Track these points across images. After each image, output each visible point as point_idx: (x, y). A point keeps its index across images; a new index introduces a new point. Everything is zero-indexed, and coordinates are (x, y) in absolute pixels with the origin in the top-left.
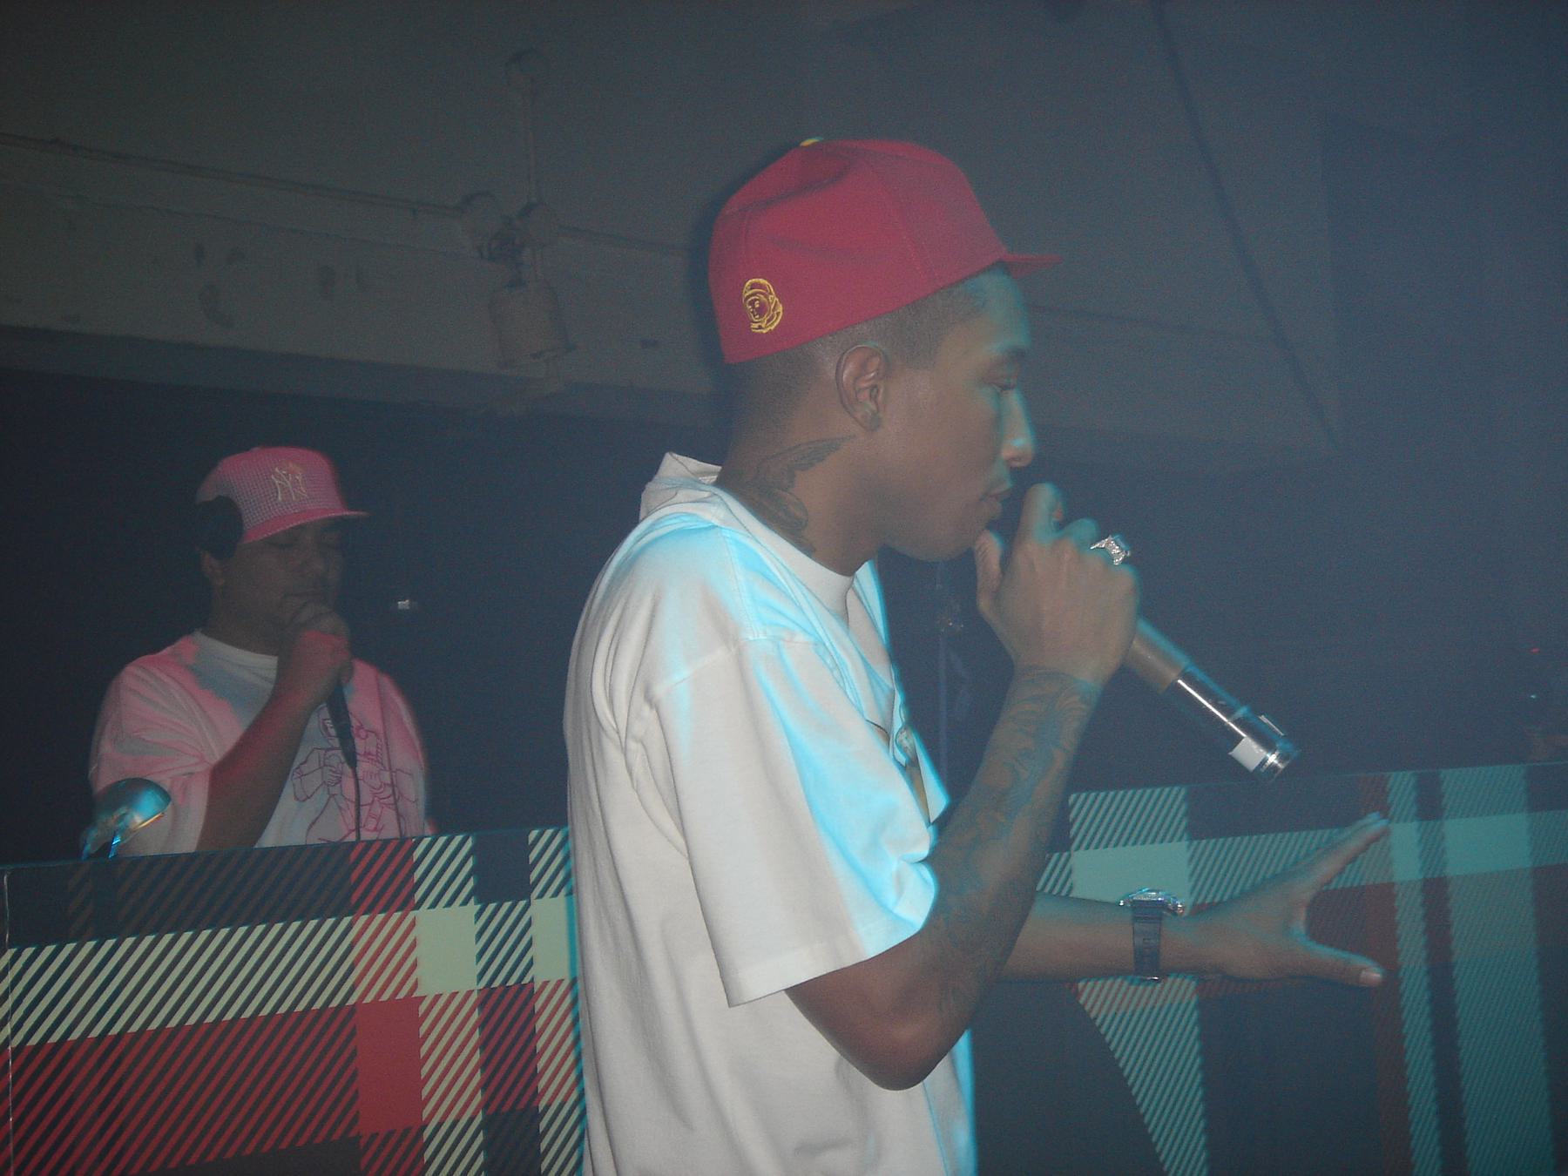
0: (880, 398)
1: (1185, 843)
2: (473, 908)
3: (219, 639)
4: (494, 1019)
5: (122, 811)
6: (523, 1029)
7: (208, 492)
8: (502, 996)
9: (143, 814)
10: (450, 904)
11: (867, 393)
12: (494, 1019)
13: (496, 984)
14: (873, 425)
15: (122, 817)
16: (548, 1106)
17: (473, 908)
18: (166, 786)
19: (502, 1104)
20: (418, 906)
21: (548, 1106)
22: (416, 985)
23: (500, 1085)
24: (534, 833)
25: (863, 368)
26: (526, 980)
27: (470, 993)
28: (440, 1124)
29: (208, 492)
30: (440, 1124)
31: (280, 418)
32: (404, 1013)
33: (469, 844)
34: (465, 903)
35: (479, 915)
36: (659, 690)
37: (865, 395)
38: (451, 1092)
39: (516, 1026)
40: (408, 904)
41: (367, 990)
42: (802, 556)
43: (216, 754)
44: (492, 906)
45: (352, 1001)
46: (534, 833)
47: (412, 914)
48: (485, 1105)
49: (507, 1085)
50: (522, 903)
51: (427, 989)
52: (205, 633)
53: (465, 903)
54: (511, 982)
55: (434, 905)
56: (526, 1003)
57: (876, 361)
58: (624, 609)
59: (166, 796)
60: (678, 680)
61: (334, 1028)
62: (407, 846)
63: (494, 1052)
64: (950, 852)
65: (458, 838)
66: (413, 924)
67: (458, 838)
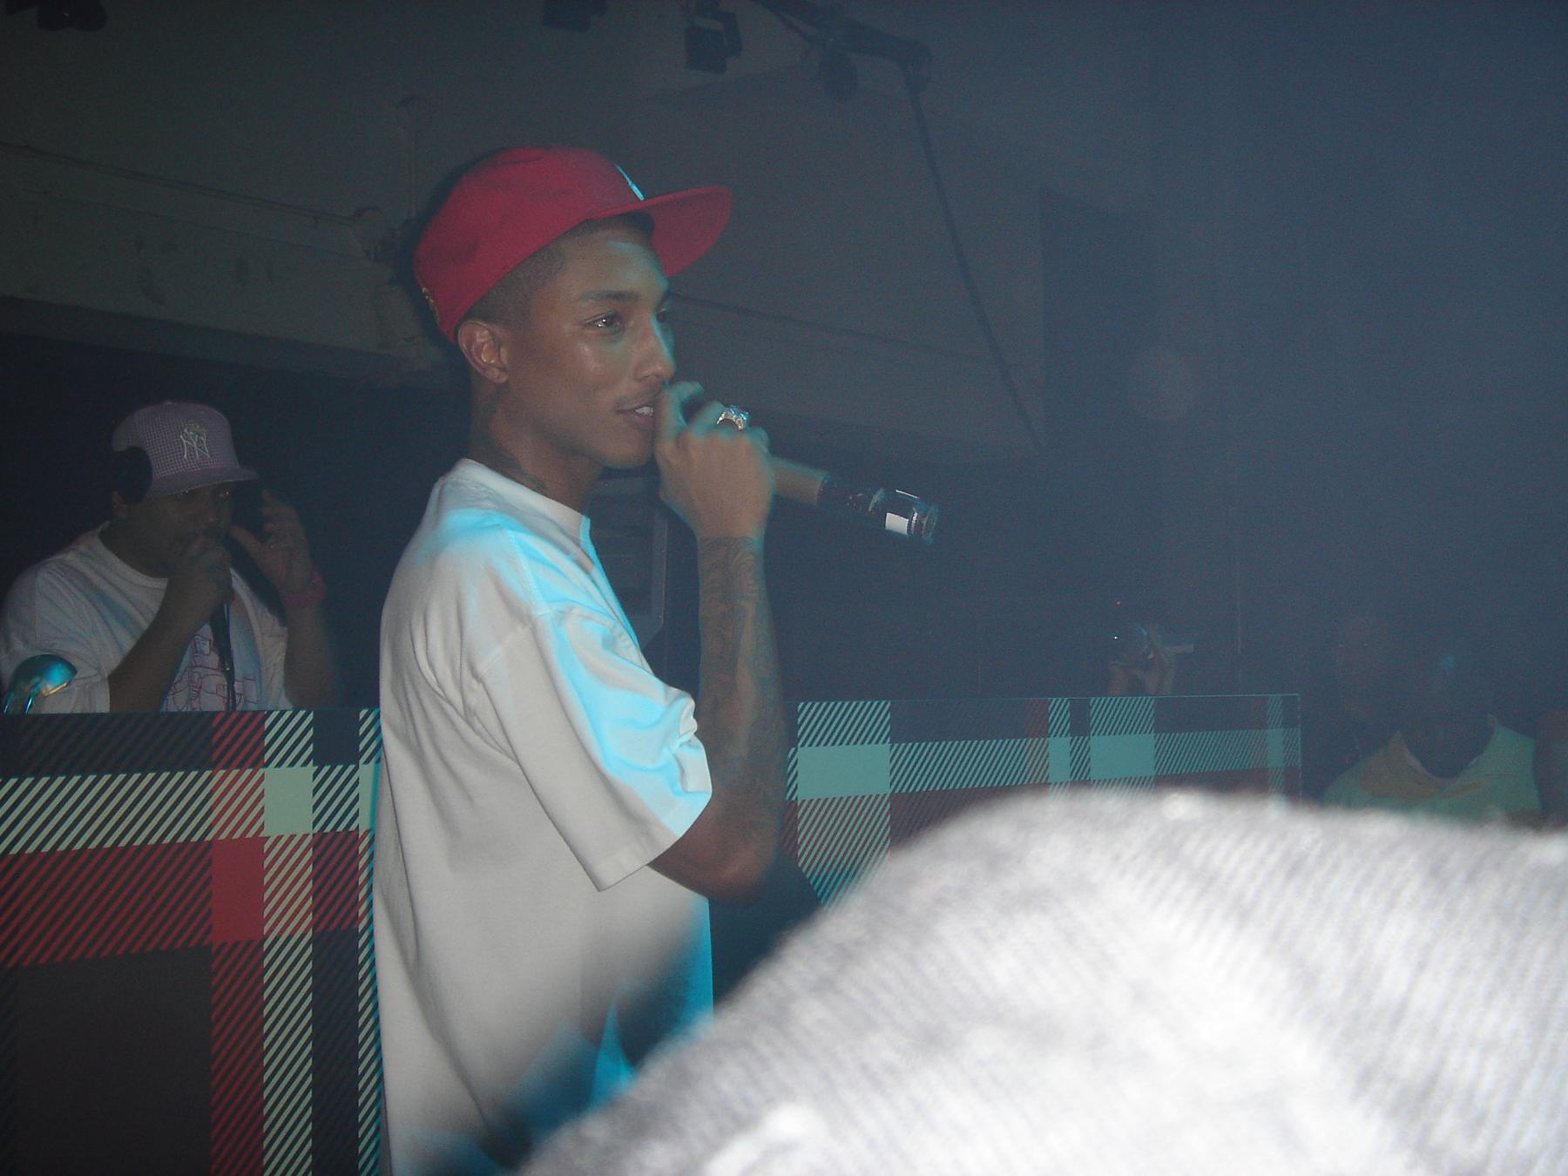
2: (311, 768)
3: (119, 555)
4: (325, 874)
5: (36, 680)
6: (349, 865)
7: (121, 443)
8: (332, 840)
9: (53, 684)
10: (292, 764)
12: (325, 874)
13: (328, 829)
15: (36, 685)
17: (311, 768)
18: (75, 663)
19: (327, 926)
20: (266, 765)
22: (262, 828)
23: (328, 877)
24: (364, 712)
26: (353, 828)
27: (306, 836)
28: (277, 939)
29: (121, 443)
30: (277, 939)
31: (173, 375)
32: (251, 850)
33: (311, 717)
36: (482, 668)
38: (287, 918)
39: (342, 866)
40: (258, 763)
41: (222, 829)
42: (660, 876)
43: (112, 660)
44: (327, 768)
45: (209, 838)
46: (364, 712)
47: (261, 771)
48: (315, 925)
49: (333, 863)
50: (351, 767)
51: (270, 832)
52: (109, 541)
53: (306, 763)
54: (340, 829)
55: (279, 765)
56: (351, 894)
58: (441, 493)
59: (73, 670)
60: (496, 656)
61: (196, 859)
62: (260, 717)
63: (324, 916)
64: (711, 734)
66: (262, 779)
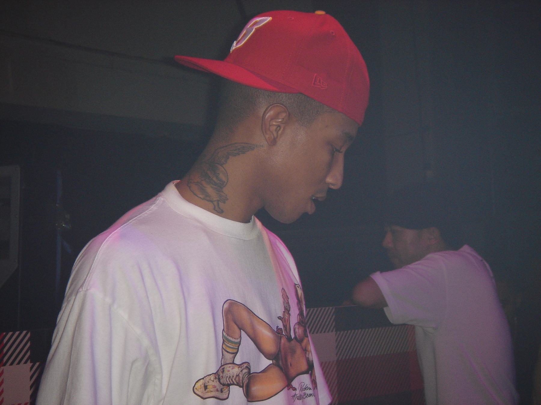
0: (280, 132)
1: (334, 332)
2: (29, 364)
3: (46, 359)
10: (19, 363)
11: (275, 128)
14: (273, 142)
16: (332, 316)
17: (29, 364)
20: (4, 365)
21: (332, 316)
25: (276, 116)
33: (29, 335)
34: (26, 363)
35: (31, 368)
37: (273, 128)
53: (26, 363)
57: (284, 115)
65: (24, 332)
67: (24, 332)
